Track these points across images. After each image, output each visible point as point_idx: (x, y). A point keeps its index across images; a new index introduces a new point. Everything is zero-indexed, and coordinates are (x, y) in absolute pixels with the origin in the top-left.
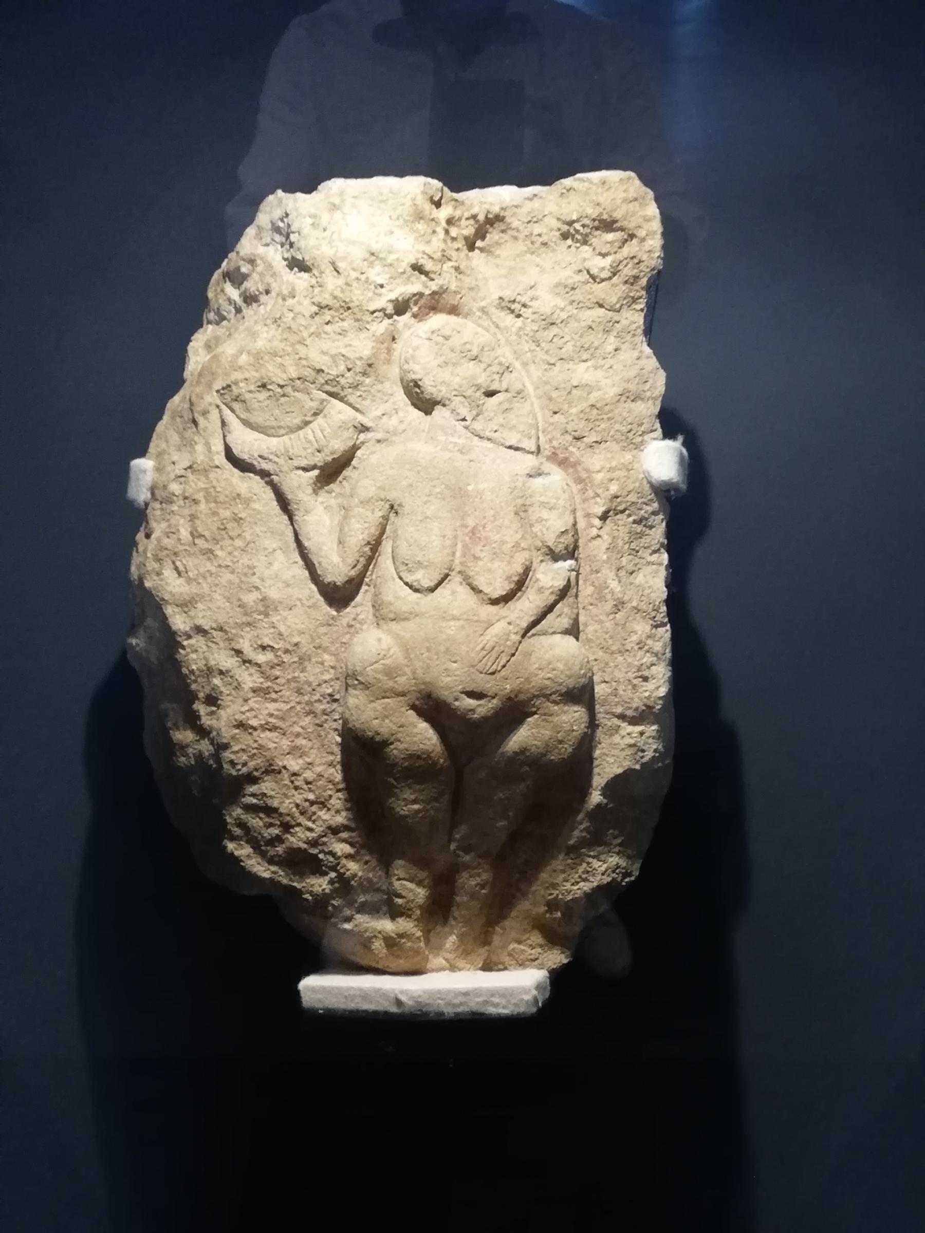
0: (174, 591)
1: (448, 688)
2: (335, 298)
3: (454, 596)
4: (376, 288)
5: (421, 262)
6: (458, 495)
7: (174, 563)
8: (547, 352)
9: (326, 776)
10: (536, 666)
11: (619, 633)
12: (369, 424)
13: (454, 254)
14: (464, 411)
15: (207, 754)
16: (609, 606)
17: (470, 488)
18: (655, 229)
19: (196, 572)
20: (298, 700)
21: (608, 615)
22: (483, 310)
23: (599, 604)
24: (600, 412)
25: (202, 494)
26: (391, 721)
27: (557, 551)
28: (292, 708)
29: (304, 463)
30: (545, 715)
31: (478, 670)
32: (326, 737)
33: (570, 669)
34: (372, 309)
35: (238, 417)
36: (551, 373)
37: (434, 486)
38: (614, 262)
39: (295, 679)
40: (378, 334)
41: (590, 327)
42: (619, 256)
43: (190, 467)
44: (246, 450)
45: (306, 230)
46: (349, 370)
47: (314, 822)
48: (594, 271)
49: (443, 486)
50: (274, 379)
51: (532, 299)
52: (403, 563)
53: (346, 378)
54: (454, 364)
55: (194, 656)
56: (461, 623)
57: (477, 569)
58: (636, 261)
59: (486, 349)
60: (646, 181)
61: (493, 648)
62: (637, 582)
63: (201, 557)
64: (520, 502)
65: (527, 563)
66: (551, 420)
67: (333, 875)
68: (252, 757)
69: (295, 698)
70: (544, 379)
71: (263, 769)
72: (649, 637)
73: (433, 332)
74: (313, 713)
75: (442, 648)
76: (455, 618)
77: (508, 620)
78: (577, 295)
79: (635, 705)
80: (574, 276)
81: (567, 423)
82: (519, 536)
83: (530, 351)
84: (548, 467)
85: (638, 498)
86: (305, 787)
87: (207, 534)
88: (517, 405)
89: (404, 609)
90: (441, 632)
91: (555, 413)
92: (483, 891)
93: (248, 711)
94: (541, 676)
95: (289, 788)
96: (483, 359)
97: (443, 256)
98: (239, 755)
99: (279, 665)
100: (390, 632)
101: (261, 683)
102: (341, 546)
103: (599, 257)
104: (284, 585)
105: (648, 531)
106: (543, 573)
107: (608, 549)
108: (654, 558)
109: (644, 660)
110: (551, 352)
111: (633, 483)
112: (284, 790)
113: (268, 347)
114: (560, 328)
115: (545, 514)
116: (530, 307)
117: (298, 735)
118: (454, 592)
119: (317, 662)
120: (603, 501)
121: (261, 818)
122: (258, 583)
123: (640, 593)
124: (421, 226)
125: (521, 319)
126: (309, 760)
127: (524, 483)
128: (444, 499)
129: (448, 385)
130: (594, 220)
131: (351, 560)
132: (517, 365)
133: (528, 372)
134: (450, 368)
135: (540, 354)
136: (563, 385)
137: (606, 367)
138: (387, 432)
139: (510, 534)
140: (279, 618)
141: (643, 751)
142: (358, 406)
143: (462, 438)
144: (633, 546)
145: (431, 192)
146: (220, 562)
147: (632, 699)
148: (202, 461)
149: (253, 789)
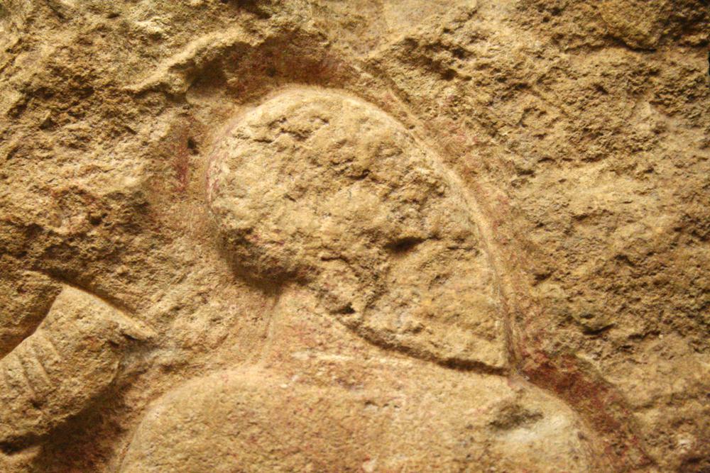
2: (58, 71)
8: (512, 146)
12: (148, 332)
14: (345, 291)
22: (374, 67)
36: (525, 192)
40: (154, 138)
46: (96, 222)
51: (474, 39)
54: (319, 191)
66: (534, 293)
70: (513, 203)
73: (271, 125)
83: (477, 145)
84: (535, 399)
88: (460, 264)
91: (541, 278)
110: (522, 146)
114: (535, 94)
116: (471, 54)
127: (487, 444)
129: (310, 238)
133: (477, 190)
134: (311, 199)
135: (499, 151)
136: (554, 217)
138: (185, 348)
142: (120, 296)
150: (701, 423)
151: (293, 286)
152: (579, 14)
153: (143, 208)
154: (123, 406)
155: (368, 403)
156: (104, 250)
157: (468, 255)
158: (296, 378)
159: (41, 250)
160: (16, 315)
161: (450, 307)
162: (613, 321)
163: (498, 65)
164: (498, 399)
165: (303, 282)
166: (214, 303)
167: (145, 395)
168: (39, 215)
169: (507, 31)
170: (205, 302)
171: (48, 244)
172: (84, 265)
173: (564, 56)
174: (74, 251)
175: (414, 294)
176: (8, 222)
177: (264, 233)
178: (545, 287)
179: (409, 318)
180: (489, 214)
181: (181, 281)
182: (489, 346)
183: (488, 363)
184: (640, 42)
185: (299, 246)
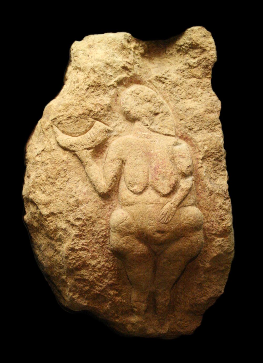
0: (41, 199)
1: (150, 230)
2: (95, 82)
3: (150, 195)
4: (110, 77)
5: (126, 65)
6: (148, 155)
7: (40, 188)
9: (105, 266)
10: (183, 219)
11: (212, 203)
12: (111, 129)
13: (137, 61)
14: (147, 122)
15: (59, 260)
16: (207, 193)
17: (152, 152)
18: (213, 47)
19: (49, 191)
20: (92, 238)
21: (207, 196)
22: (150, 81)
23: (204, 193)
24: (198, 119)
25: (49, 161)
26: (129, 244)
27: (187, 174)
28: (91, 241)
29: (87, 147)
30: (187, 237)
31: (161, 223)
32: (104, 251)
33: (195, 219)
34: (109, 85)
35: (60, 130)
36: (178, 104)
37: (138, 152)
38: (199, 60)
39: (91, 230)
40: (112, 94)
41: (191, 86)
42: (200, 58)
43: (43, 150)
45: (81, 56)
46: (102, 109)
47: (102, 283)
48: (191, 64)
49: (142, 152)
51: (168, 76)
52: (129, 183)
53: (101, 113)
55: (51, 224)
56: (154, 205)
57: (158, 184)
58: (207, 59)
59: (153, 97)
60: (208, 29)
61: (166, 214)
62: (217, 183)
63: (51, 185)
64: (171, 156)
65: (176, 180)
66: (180, 123)
67: (110, 302)
68: (77, 261)
69: (92, 237)
70: (176, 107)
71: (82, 265)
72: (224, 204)
73: (132, 92)
74: (99, 242)
75: (147, 215)
76: (151, 203)
77: (171, 202)
78: (185, 73)
79: (220, 230)
80: (183, 66)
81: (186, 124)
82: (172, 169)
83: (169, 96)
84: (180, 141)
85: (215, 151)
86: (98, 270)
87: (52, 176)
88: (167, 117)
89: (131, 201)
90: (146, 209)
91: (181, 120)
92: (167, 303)
93: (74, 244)
94: (185, 223)
95: (92, 272)
96: (152, 101)
97: (134, 62)
98: (72, 261)
99: (84, 225)
100: (126, 210)
101: (78, 233)
102: (105, 178)
103: (192, 59)
105: (219, 163)
106: (182, 183)
107: (206, 171)
108: (222, 173)
109: (222, 213)
110: (177, 96)
111: (213, 145)
112: (90, 273)
113: (70, 102)
114: (179, 86)
115: (181, 160)
116: (168, 79)
117: (94, 251)
118: (149, 193)
119: (99, 223)
120: (202, 153)
121: (81, 283)
122: (74, 194)
123: (219, 187)
124: (124, 52)
125: (165, 84)
126: (98, 260)
128: (142, 157)
130: (190, 45)
131: (109, 183)
132: (165, 102)
133: (169, 104)
134: (140, 105)
135: (173, 97)
136: (183, 109)
137: (198, 101)
138: (118, 132)
139: (169, 168)
140: (83, 207)
141: (224, 247)
142: (106, 123)
143: (147, 133)
144: (215, 169)
145: (127, 38)
146: (58, 187)
147: (219, 228)
149: (78, 273)
150: (209, 144)
152: (188, 72)
157: (168, 116)
158: (138, 137)
162: (194, 127)
163: (173, 81)
164: (174, 141)
169: (174, 75)
173: (185, 79)
178: (182, 121)
180: (171, 108)
182: (172, 132)
183: (172, 135)
184: (199, 77)
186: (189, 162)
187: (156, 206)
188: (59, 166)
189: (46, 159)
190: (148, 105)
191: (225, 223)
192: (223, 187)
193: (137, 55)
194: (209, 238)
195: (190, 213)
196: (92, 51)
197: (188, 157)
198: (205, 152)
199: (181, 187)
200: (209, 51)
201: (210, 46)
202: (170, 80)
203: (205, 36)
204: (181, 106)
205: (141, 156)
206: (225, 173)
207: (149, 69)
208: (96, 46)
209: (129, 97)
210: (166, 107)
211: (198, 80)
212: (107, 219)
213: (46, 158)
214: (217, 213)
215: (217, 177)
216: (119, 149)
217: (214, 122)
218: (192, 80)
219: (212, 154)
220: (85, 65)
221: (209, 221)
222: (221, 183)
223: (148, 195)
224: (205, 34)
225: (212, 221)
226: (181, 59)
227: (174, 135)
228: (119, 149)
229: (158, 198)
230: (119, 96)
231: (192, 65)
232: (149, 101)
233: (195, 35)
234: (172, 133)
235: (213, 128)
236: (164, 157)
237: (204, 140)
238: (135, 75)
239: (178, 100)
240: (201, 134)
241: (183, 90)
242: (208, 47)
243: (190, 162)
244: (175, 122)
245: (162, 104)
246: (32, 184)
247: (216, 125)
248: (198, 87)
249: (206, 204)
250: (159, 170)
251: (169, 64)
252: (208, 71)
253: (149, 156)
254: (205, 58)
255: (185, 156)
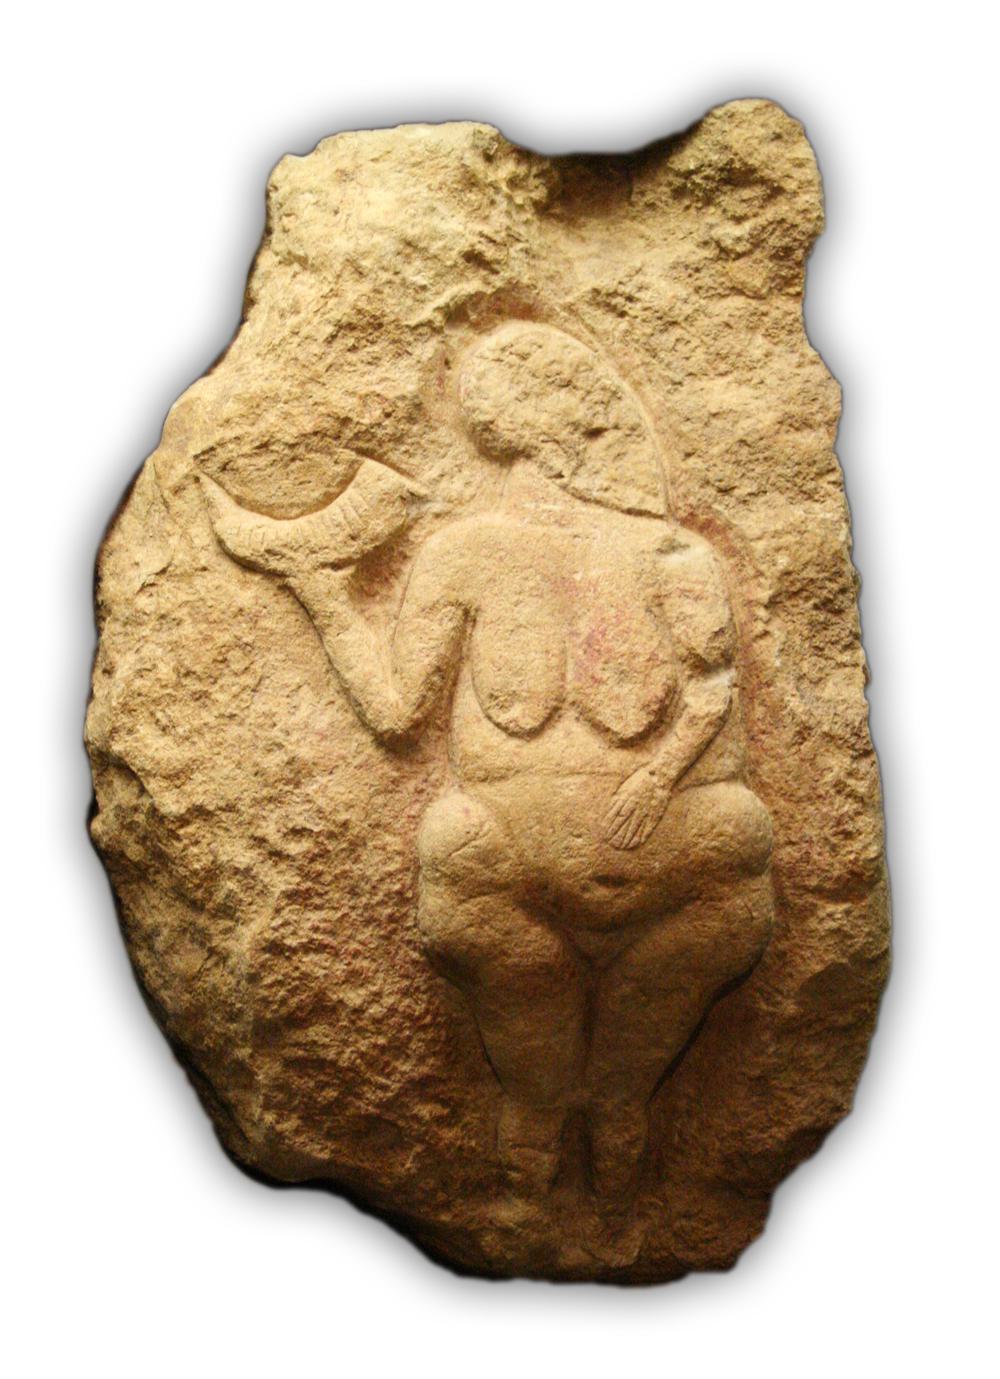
0: (158, 756)
1: (570, 874)
2: (359, 312)
3: (571, 740)
4: (417, 292)
5: (479, 247)
6: (562, 588)
7: (152, 714)
9: (401, 1009)
10: (695, 831)
11: (806, 772)
12: (423, 491)
13: (522, 230)
14: (559, 463)
15: (225, 989)
16: (788, 735)
17: (578, 577)
18: (810, 177)
19: (188, 727)
20: (351, 904)
21: (789, 746)
22: (570, 309)
23: (775, 732)
24: (752, 451)
25: (185, 610)
26: (492, 927)
27: (710, 660)
28: (345, 915)
29: (333, 557)
30: (711, 899)
31: (612, 846)
32: (397, 953)
33: (743, 832)
34: (413, 322)
35: (228, 492)
36: (676, 397)
37: (526, 579)
38: (755, 229)
39: (345, 874)
40: (424, 358)
41: (728, 325)
42: (761, 221)
43: (163, 571)
44: (461, 737)
45: (308, 213)
46: (388, 415)
47: (388, 1076)
48: (728, 243)
49: (538, 577)
50: (279, 436)
51: (640, 289)
52: (491, 696)
53: (385, 428)
55: (195, 850)
56: (584, 778)
57: (599, 697)
58: (786, 226)
59: (582, 368)
61: (632, 812)
62: (826, 695)
63: (192, 704)
64: (651, 591)
65: (670, 682)
66: (683, 466)
67: (419, 1148)
68: (293, 992)
69: (348, 902)
70: (668, 405)
71: (311, 1007)
72: (850, 774)
73: (503, 350)
74: (375, 920)
75: (559, 817)
76: (573, 772)
77: (649, 768)
78: (705, 279)
79: (836, 873)
80: (697, 250)
81: (707, 470)
82: (655, 643)
83: (643, 364)
84: (684, 535)
85: (818, 572)
86: (371, 1028)
87: (198, 669)
88: (633, 446)
89: (498, 763)
90: (555, 794)
91: (688, 455)
92: (634, 1152)
93: (282, 925)
94: (702, 846)
95: (349, 1032)
96: (579, 384)
97: (509, 235)
98: (274, 990)
99: (321, 856)
100: (480, 798)
101: (298, 884)
102: (397, 676)
103: (731, 223)
104: (318, 738)
105: (834, 619)
106: (693, 694)
107: (782, 650)
109: (846, 808)
110: (674, 365)
111: (809, 551)
112: (343, 1036)
113: (265, 389)
114: (682, 328)
115: (688, 608)
116: (638, 300)
117: (356, 954)
118: (568, 734)
119: (375, 847)
120: (769, 582)
121: (310, 1076)
122: (281, 738)
123: (832, 711)
124: (473, 196)
125: (627, 318)
126: (374, 989)
128: (541, 596)
130: (722, 170)
131: (414, 697)
132: (626, 386)
133: (642, 396)
134: (533, 401)
135: (659, 369)
136: (697, 414)
137: (753, 382)
138: (450, 501)
139: (644, 640)
140: (315, 787)
141: (851, 937)
142: (404, 466)
143: (560, 504)
144: (817, 642)
145: (484, 143)
146: (222, 710)
147: (832, 865)
148: (182, 562)
149: (298, 1036)
150: (794, 549)
151: (522, 460)
152: (713, 272)
153: (418, 406)
154: (408, 540)
155: (575, 536)
156: (394, 434)
157: (639, 440)
158: (526, 521)
159: (351, 435)
160: (333, 479)
161: (628, 474)
162: (737, 484)
163: (657, 308)
164: (661, 534)
165: (529, 457)
166: (466, 472)
167: (423, 533)
168: (350, 411)
169: (663, 284)
170: (460, 471)
171: (356, 431)
172: (380, 445)
173: (703, 302)
174: (374, 436)
175: (604, 465)
176: (329, 415)
177: (502, 424)
178: (691, 461)
179: (600, 481)
180: (651, 412)
181: (444, 456)
182: (653, 500)
183: (654, 511)
184: (755, 292)
185: (527, 433)
186: (717, 615)
187: (592, 782)
188: (226, 629)
189: (173, 604)
190: (563, 399)
191: (857, 846)
192: (849, 711)
193: (520, 208)
194: (795, 904)
195: (723, 809)
196: (350, 192)
197: (716, 595)
198: (780, 579)
199: (688, 709)
200: (795, 194)
201: (797, 174)
202: (647, 305)
203: (778, 137)
204: (688, 404)
205: (535, 593)
206: (855, 659)
207: (567, 261)
208: (364, 176)
209: (490, 369)
210: (633, 407)
211: (754, 303)
212: (406, 833)
213: (173, 600)
214: (825, 810)
215: (827, 671)
216: (451, 564)
217: (815, 462)
218: (731, 305)
219: (807, 584)
220: (325, 245)
221: (794, 840)
222: (839, 694)
223: (564, 742)
224: (778, 130)
225: (807, 838)
226: (687, 225)
227: (661, 513)
228: (451, 564)
229: (601, 752)
230: (452, 365)
231: (730, 247)
232: (568, 384)
233: (742, 131)
234: (656, 505)
235: (811, 485)
236: (624, 596)
237: (776, 532)
238: (514, 286)
239: (678, 379)
240: (763, 508)
241: (695, 342)
242: (790, 180)
243: (722, 614)
244: (666, 464)
245: (615, 395)
246: (121, 700)
247: (820, 475)
248: (752, 329)
249: (785, 775)
250: (606, 645)
251: (642, 243)
252: (790, 268)
253: (566, 592)
254: (778, 219)
255: (705, 594)
